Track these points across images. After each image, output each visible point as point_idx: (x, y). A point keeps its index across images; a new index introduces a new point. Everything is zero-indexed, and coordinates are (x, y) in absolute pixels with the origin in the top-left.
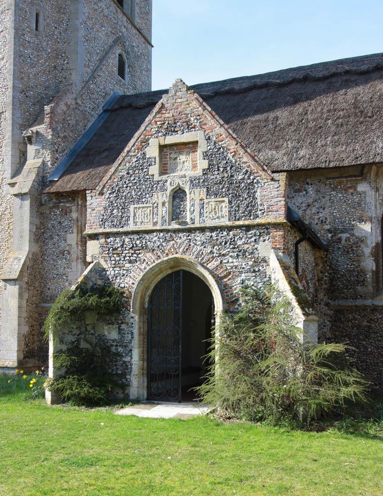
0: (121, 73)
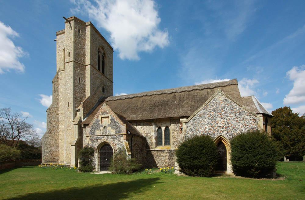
0: (103, 91)
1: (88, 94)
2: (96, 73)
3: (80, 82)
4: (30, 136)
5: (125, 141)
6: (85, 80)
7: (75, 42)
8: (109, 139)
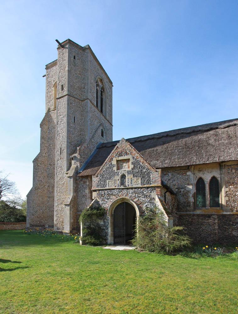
0: (102, 135)
4: (12, 195)
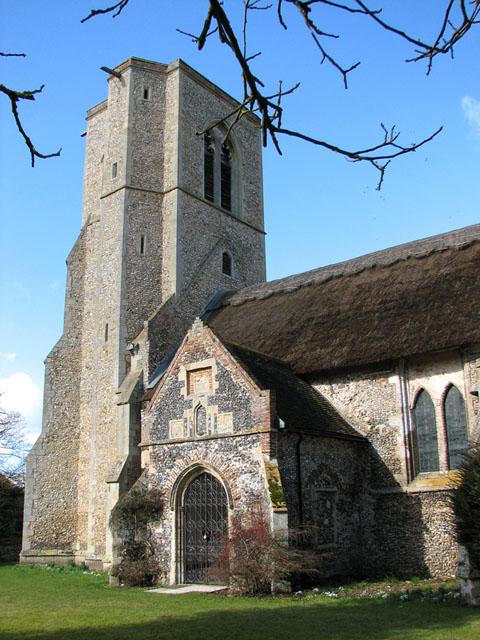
0: (227, 269)
1: (170, 287)
2: (199, 212)
3: (144, 251)
5: (268, 457)
6: (160, 242)
7: (132, 131)
8: (210, 455)
